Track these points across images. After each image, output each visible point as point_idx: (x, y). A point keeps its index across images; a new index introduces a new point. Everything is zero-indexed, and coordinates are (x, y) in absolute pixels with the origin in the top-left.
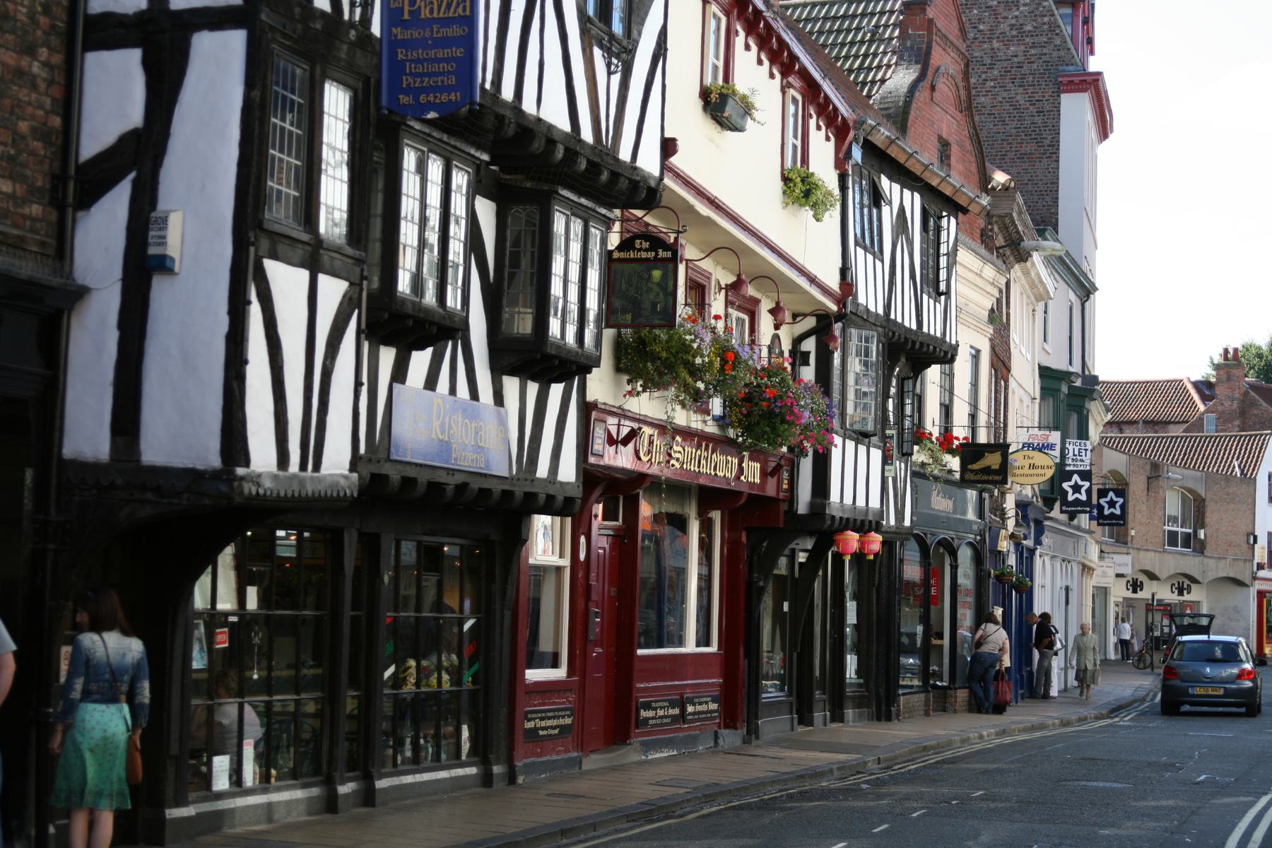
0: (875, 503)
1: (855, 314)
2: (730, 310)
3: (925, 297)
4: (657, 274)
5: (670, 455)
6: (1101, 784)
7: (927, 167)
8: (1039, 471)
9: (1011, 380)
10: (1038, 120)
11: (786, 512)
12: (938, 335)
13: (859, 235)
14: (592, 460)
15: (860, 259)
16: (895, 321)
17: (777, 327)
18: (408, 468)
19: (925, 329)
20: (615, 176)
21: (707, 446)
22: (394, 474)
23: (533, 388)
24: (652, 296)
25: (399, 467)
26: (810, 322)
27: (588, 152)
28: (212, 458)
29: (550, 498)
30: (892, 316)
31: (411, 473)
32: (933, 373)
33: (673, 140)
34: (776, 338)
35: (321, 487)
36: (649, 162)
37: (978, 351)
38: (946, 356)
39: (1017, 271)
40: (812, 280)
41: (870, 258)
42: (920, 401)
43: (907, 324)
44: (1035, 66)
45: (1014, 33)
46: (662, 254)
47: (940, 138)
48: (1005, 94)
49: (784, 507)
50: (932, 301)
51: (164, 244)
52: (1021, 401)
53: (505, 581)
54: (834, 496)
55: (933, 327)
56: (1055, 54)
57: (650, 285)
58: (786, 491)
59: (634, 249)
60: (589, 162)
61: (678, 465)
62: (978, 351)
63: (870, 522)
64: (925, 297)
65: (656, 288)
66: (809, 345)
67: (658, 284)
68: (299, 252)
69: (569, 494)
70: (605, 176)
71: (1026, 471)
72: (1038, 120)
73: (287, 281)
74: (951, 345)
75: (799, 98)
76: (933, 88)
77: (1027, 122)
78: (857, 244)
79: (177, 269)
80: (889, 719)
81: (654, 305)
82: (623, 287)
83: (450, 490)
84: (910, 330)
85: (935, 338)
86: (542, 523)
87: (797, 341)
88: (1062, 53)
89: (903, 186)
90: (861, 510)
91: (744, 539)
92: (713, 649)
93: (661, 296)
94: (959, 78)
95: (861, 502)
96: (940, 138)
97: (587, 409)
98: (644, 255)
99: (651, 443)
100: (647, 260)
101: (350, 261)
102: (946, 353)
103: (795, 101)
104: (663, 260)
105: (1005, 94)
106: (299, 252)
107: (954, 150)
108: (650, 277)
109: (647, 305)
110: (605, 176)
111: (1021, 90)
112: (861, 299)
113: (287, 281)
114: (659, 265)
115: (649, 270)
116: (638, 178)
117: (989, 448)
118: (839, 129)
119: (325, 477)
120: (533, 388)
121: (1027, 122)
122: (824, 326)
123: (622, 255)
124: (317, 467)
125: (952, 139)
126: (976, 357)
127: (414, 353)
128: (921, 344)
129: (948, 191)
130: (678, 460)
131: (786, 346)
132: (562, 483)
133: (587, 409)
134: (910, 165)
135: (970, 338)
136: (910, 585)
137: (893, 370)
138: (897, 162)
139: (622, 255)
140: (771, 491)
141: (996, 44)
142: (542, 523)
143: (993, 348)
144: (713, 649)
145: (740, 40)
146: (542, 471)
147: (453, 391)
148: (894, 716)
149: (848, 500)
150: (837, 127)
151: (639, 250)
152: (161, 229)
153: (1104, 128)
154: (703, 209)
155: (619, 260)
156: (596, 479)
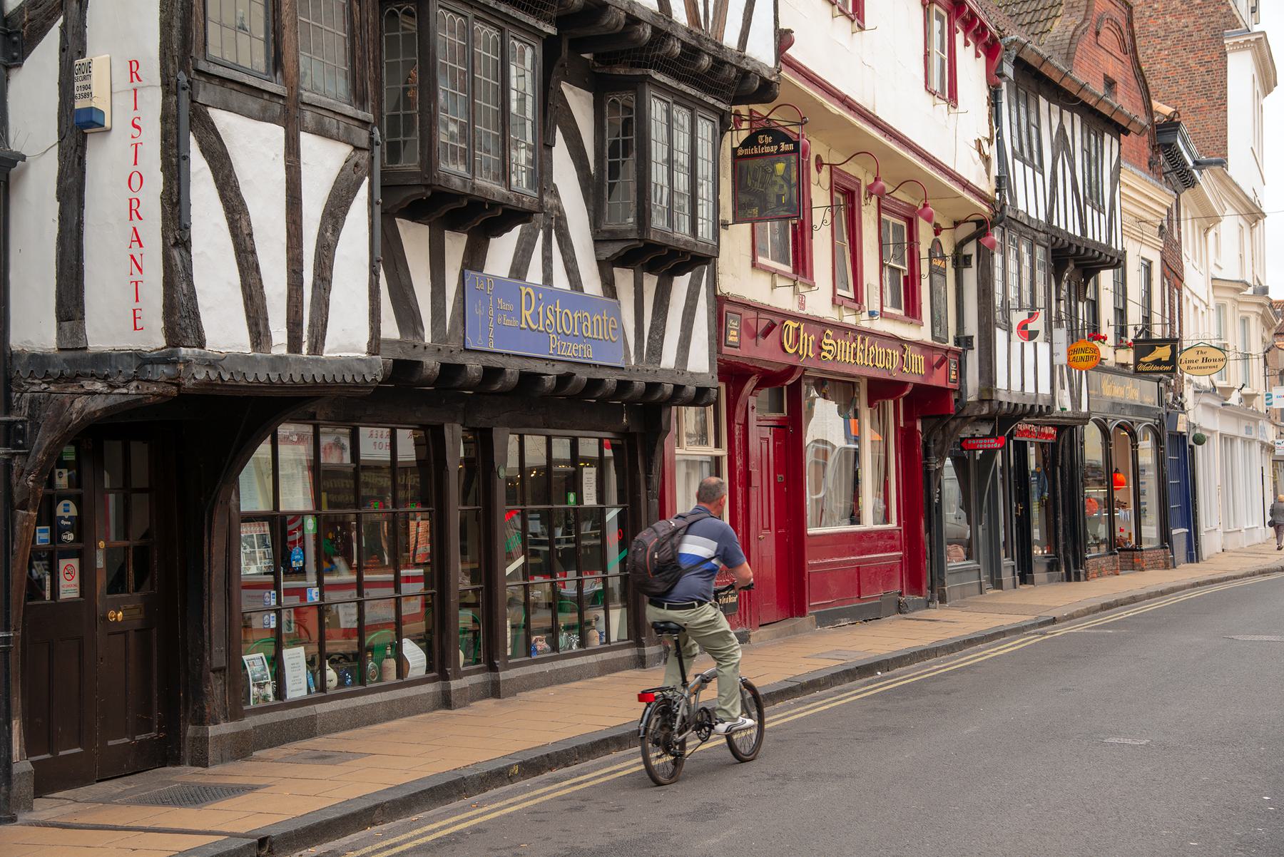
0: (1044, 389)
1: (1015, 220)
2: (884, 216)
3: (1089, 209)
4: (780, 167)
5: (821, 348)
6: (1265, 638)
7: (1083, 86)
8: (1212, 364)
9: (1184, 288)
10: (1208, 78)
11: (956, 401)
12: (1104, 241)
13: (1017, 148)
14: (725, 350)
15: (1019, 171)
16: (1058, 228)
17: (937, 233)
18: (491, 357)
19: (1090, 236)
20: (719, 63)
21: (863, 340)
22: (474, 366)
23: (650, 283)
24: (776, 189)
25: (483, 358)
26: (970, 228)
27: (683, 36)
28: (154, 339)
29: (678, 388)
30: (1055, 223)
31: (496, 362)
32: (1106, 278)
33: (789, 32)
34: (936, 244)
35: (318, 373)
36: (761, 51)
37: (1150, 262)
38: (1117, 262)
39: (1186, 195)
40: (966, 185)
41: (1029, 170)
42: (1094, 306)
43: (1070, 230)
44: (1203, 33)
45: (1185, 7)
46: (784, 147)
47: (1106, 77)
48: (1178, 60)
49: (954, 396)
50: (1096, 214)
51: (89, 95)
52: (1196, 308)
53: (648, 471)
54: (1001, 383)
55: (1097, 232)
56: (1222, 20)
57: (774, 178)
58: (955, 381)
59: (757, 144)
60: (684, 44)
61: (830, 357)
62: (1150, 262)
63: (1040, 407)
64: (1089, 209)
65: (781, 182)
66: (971, 249)
67: (782, 177)
68: (277, 108)
69: (701, 385)
70: (706, 62)
71: (1200, 364)
72: (1208, 78)
73: (253, 143)
74: (1116, 251)
75: (945, 14)
76: (1097, 33)
77: (1198, 80)
78: (1014, 156)
79: (107, 124)
80: (1078, 579)
81: (779, 197)
82: (749, 183)
83: (549, 382)
84: (1075, 236)
85: (1099, 244)
86: (689, 418)
87: (959, 246)
88: (1227, 20)
89: (1062, 108)
90: (1030, 396)
91: (919, 427)
92: (893, 525)
93: (785, 188)
94: (1123, 24)
95: (1030, 389)
96: (1106, 77)
97: (720, 304)
98: (767, 150)
99: (798, 337)
100: (771, 154)
101: (356, 123)
102: (1112, 258)
103: (940, 17)
104: (785, 152)
105: (1178, 60)
106: (277, 108)
107: (1120, 87)
108: (774, 170)
109: (773, 199)
110: (706, 62)
111: (1191, 55)
112: (1021, 206)
113: (253, 143)
114: (782, 157)
115: (773, 163)
116: (749, 68)
117: (1162, 342)
118: (990, 48)
119: (332, 361)
120: (650, 283)
121: (1198, 80)
122: (983, 228)
123: (747, 151)
124: (317, 346)
125: (1119, 78)
126: (1148, 267)
127: (492, 240)
128: (1086, 249)
129: (1105, 110)
130: (829, 352)
131: (948, 250)
132: (692, 374)
133: (720, 304)
134: (1065, 84)
135: (1139, 252)
136: (1095, 469)
137: (1062, 276)
138: (1054, 82)
139: (747, 151)
140: (938, 380)
141: (1169, 19)
142: (689, 418)
143: (1163, 260)
144: (893, 525)
145: (960, 37)
146: (669, 359)
147: (548, 278)
148: (1082, 577)
149: (1016, 386)
150: (986, 44)
151: (763, 145)
152: (85, 78)
153: (1267, 79)
154: (835, 108)
155: (744, 157)
156: (733, 373)
